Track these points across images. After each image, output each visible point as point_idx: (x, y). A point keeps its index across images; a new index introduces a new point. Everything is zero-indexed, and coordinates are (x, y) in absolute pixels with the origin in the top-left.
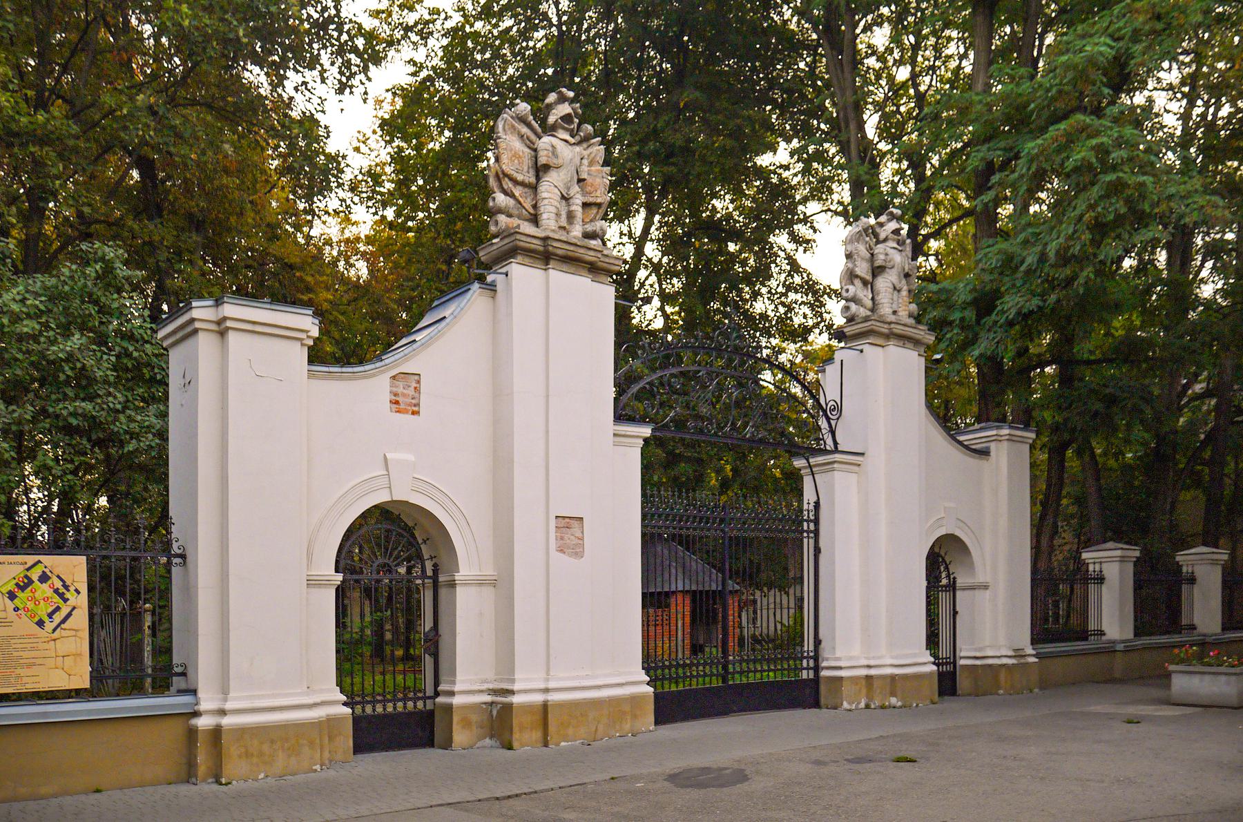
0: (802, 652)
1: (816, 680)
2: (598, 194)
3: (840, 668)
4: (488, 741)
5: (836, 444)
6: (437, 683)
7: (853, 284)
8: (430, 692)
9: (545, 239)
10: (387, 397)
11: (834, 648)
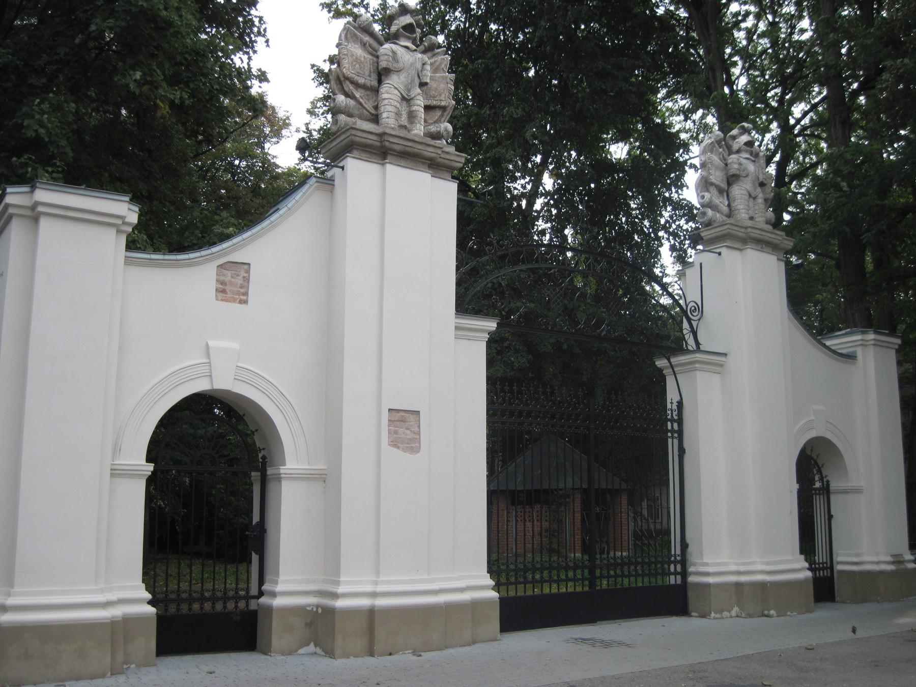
0: (670, 556)
1: (684, 587)
2: (443, 97)
3: (707, 574)
4: (311, 648)
5: (697, 343)
6: (261, 582)
7: (708, 191)
8: (254, 591)
9: (381, 135)
10: (212, 285)
11: (701, 553)
